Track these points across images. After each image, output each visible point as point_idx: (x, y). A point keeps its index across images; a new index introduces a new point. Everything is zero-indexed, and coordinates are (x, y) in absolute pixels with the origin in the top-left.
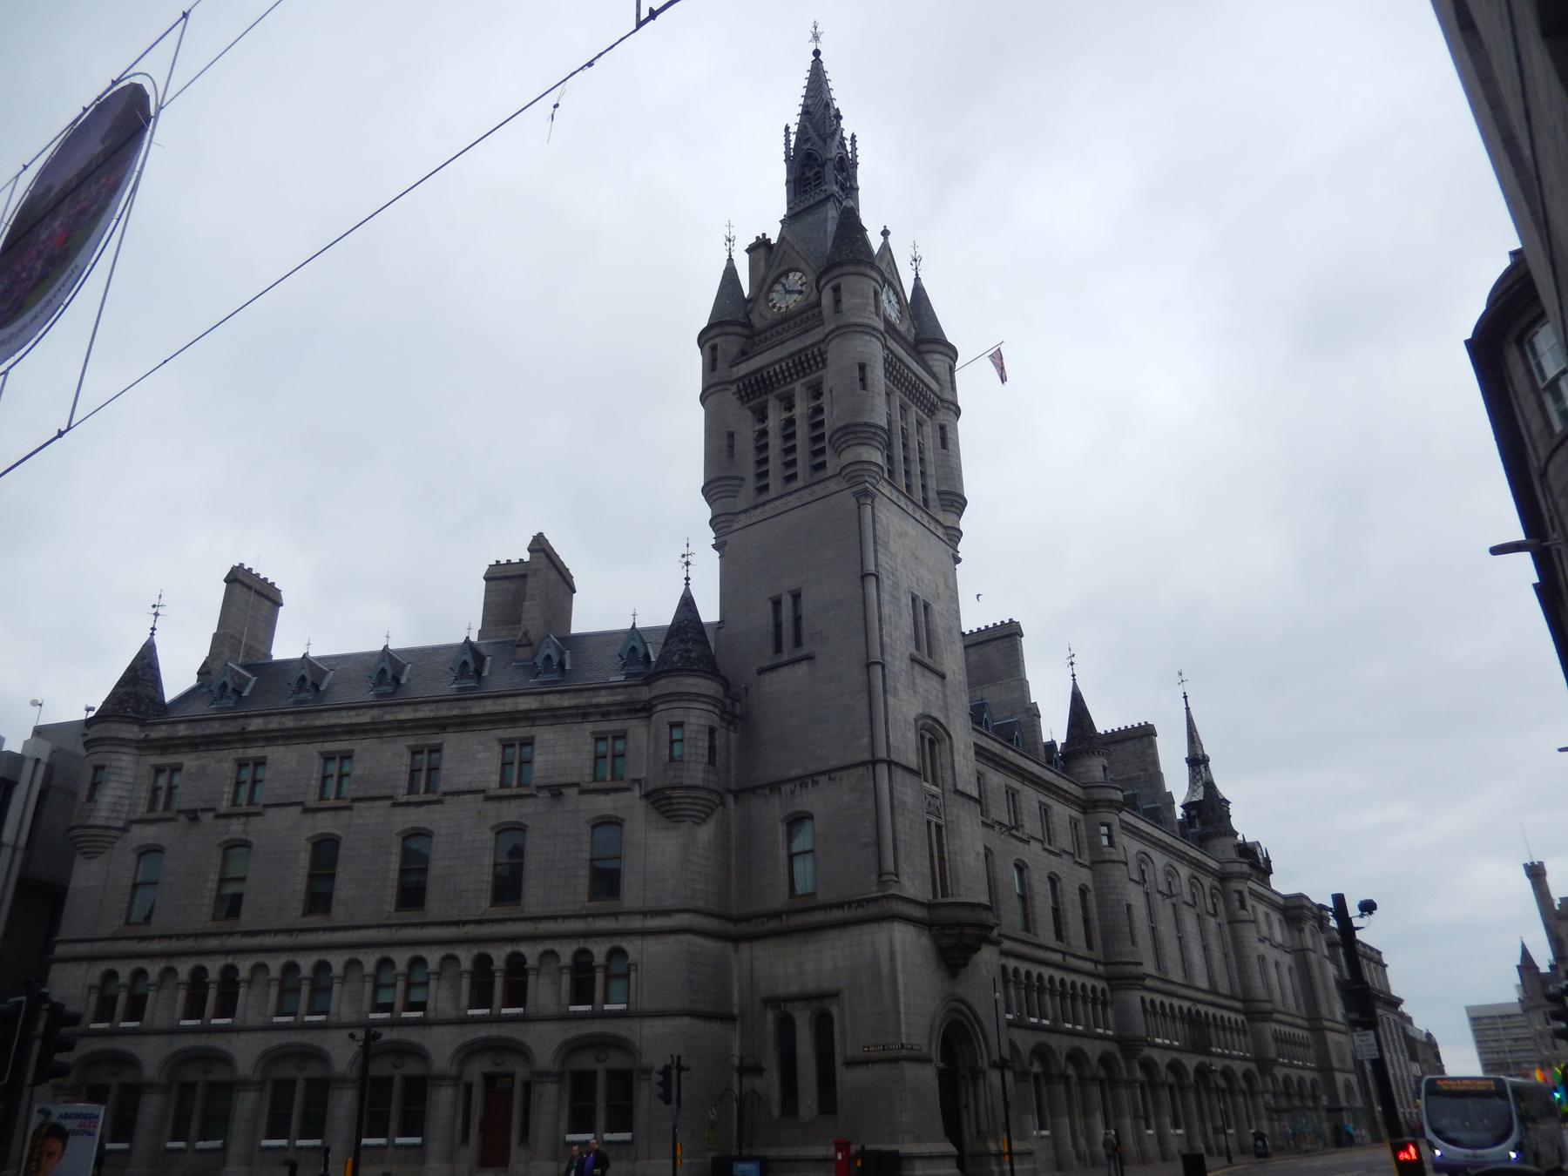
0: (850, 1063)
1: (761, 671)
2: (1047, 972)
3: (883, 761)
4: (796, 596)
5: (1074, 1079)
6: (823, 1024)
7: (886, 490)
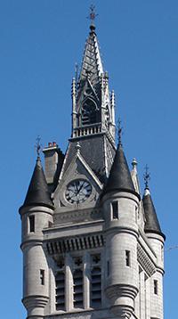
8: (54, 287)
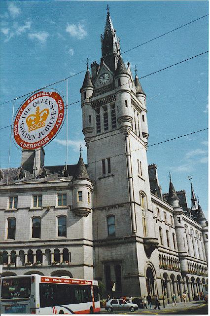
0: (125, 278)
1: (100, 179)
2: (166, 255)
3: (133, 202)
4: (109, 160)
5: (171, 281)
6: (118, 270)
7: (131, 132)
8: (96, 122)
